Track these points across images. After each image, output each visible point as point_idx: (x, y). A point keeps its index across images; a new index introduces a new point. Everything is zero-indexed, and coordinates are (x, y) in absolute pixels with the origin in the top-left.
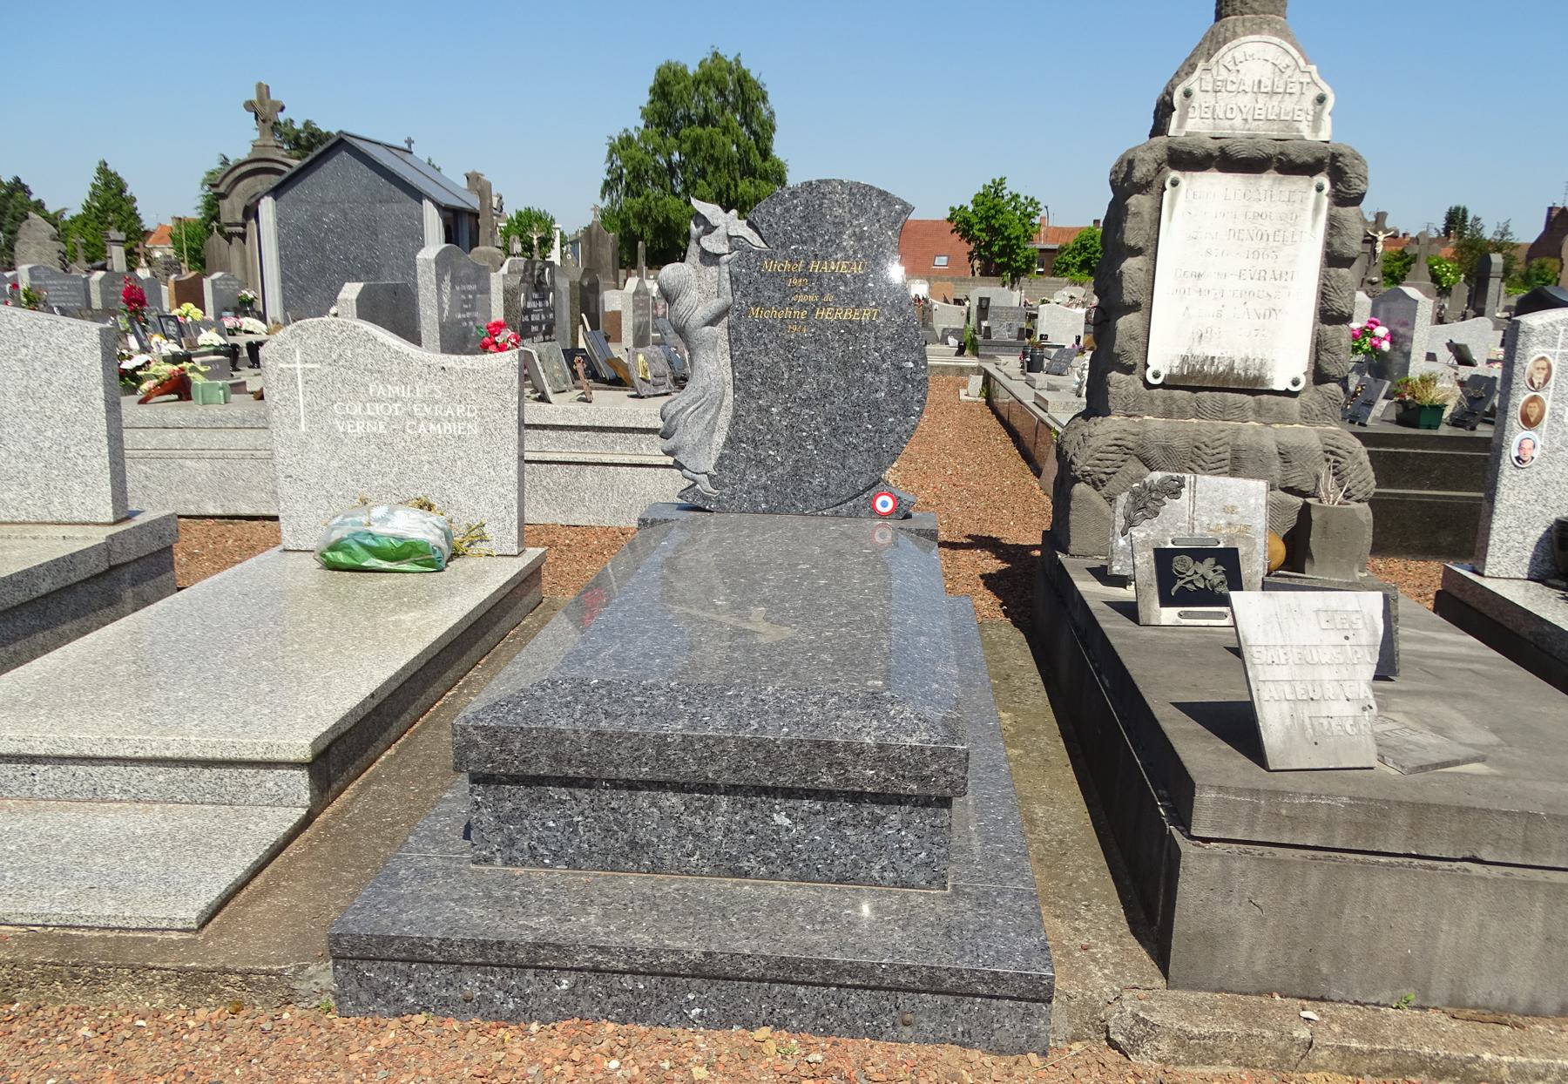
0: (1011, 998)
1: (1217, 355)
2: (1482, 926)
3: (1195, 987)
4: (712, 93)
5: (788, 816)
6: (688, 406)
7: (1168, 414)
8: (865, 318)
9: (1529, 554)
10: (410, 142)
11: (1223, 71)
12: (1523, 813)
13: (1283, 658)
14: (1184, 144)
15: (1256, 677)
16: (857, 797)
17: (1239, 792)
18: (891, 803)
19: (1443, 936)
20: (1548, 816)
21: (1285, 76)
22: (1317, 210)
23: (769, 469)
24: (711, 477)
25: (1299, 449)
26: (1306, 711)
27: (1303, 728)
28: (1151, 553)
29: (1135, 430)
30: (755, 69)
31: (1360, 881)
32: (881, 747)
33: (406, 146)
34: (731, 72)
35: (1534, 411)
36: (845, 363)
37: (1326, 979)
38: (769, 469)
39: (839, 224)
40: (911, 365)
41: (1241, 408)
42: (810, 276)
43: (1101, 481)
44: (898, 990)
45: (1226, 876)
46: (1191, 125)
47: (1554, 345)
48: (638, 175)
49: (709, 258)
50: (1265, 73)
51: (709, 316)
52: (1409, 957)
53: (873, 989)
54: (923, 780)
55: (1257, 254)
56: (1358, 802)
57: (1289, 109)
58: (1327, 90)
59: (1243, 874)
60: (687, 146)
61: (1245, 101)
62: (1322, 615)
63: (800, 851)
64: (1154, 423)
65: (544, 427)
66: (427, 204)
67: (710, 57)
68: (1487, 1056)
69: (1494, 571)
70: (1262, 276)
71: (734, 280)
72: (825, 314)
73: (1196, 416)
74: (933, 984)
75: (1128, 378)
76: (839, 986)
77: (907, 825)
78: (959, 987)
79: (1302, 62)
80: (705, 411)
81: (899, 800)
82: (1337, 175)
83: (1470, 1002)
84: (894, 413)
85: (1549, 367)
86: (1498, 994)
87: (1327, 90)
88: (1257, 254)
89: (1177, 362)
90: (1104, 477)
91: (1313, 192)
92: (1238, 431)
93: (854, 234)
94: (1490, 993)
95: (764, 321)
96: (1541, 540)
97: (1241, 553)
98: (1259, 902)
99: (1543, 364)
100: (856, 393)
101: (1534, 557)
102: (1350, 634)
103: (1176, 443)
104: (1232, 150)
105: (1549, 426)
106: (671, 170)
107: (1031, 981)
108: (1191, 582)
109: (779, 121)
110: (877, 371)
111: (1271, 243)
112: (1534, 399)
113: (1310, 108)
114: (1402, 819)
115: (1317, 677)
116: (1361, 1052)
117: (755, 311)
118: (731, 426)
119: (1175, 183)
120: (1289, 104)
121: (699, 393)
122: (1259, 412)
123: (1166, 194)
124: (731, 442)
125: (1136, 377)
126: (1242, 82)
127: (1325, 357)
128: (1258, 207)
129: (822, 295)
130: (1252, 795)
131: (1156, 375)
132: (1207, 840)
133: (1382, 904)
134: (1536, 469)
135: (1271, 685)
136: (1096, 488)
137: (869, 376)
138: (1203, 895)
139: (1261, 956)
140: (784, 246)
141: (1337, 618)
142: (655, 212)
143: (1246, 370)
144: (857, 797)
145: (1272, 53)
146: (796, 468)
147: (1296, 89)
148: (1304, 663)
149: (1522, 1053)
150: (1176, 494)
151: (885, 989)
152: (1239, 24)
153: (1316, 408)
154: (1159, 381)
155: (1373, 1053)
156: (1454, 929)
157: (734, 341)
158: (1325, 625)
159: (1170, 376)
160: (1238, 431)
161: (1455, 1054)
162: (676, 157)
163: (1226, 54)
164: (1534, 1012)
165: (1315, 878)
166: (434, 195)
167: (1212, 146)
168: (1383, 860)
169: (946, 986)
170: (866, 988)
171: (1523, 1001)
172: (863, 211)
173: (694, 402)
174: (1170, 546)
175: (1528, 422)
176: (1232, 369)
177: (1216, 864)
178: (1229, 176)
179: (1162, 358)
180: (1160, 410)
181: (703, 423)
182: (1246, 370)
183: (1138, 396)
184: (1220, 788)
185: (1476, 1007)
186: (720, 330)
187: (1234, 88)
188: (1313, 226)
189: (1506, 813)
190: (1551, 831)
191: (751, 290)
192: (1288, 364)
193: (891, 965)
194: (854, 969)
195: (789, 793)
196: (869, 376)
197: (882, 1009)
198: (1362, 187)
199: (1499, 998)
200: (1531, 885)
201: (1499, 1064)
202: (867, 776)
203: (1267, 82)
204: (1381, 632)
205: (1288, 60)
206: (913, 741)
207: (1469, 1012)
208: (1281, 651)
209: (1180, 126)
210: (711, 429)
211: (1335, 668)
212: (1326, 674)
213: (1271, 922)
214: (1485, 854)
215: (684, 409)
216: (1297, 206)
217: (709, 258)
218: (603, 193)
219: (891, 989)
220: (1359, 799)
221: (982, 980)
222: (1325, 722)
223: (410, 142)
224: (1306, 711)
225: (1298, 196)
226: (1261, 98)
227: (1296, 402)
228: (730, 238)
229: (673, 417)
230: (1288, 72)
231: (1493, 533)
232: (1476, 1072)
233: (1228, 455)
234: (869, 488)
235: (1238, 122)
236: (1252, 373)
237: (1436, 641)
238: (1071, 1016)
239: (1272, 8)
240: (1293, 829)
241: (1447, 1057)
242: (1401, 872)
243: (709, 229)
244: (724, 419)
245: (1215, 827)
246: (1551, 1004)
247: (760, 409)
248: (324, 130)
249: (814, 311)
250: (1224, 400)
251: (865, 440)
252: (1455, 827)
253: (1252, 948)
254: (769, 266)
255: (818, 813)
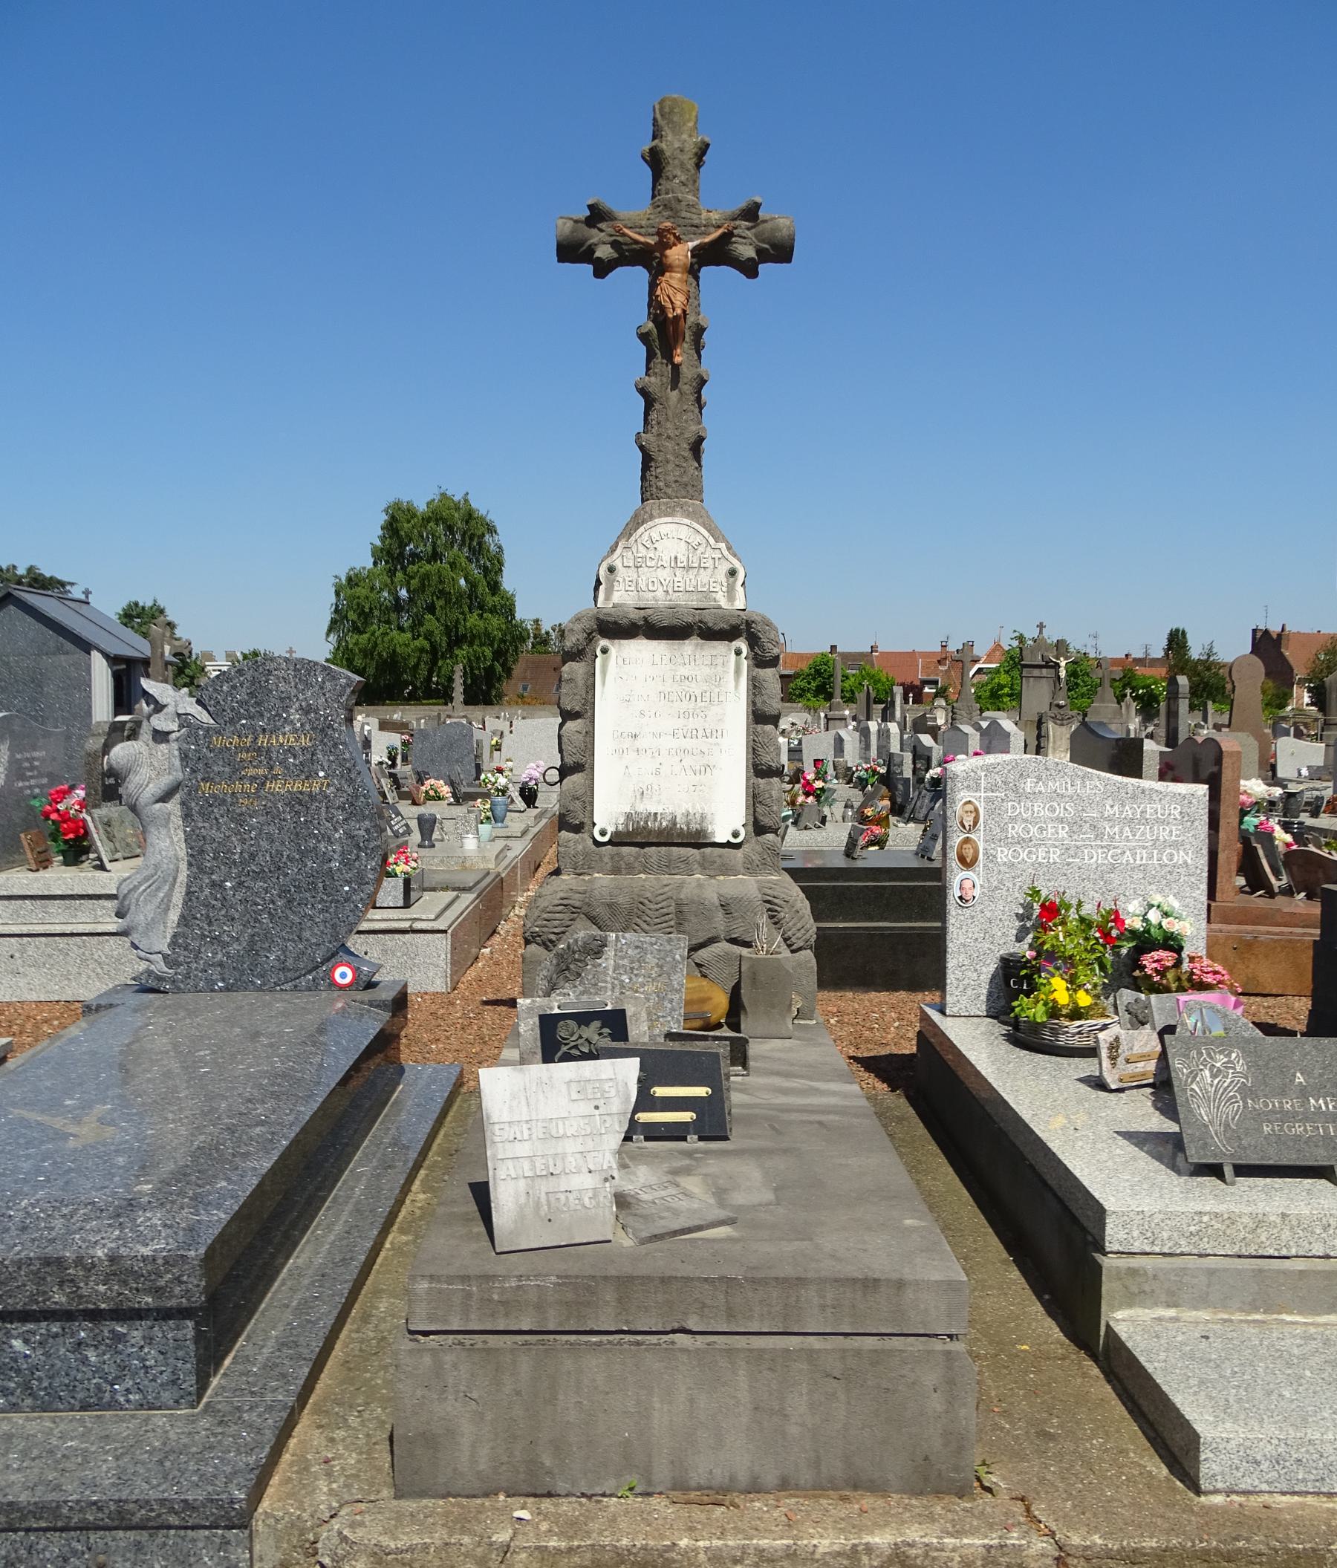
0: (205, 1528)
1: (660, 811)
2: (692, 1401)
3: (422, 1494)
4: (441, 529)
5: (26, 1341)
6: (140, 884)
7: (616, 871)
8: (316, 790)
9: (985, 991)
10: (87, 593)
11: (641, 548)
12: (721, 1278)
13: (526, 1134)
14: (609, 615)
15: (494, 1156)
16: (95, 1316)
17: (450, 1279)
18: (131, 1319)
19: (656, 1414)
20: (745, 1278)
21: (698, 552)
22: (738, 671)
23: (225, 945)
24: (165, 957)
25: (739, 900)
26: (543, 1187)
27: (538, 1205)
28: (537, 1020)
29: (581, 889)
30: (480, 505)
31: (568, 1364)
32: (113, 1259)
33: (83, 597)
34: (457, 508)
35: (969, 854)
36: (297, 834)
37: (549, 1473)
38: (225, 945)
39: (285, 700)
40: (362, 832)
41: (686, 861)
42: (259, 750)
43: (551, 941)
44: (88, 1529)
45: (438, 1371)
46: (622, 598)
47: (978, 790)
48: (365, 616)
49: (160, 736)
50: (681, 551)
51: (159, 793)
52: (628, 1440)
53: (62, 1530)
54: (158, 1292)
55: (687, 714)
56: (566, 1281)
57: (705, 581)
58: (737, 565)
59: (455, 1366)
60: (415, 583)
61: (664, 575)
62: (574, 1086)
63: (40, 1379)
64: (602, 880)
65: (99, 897)
66: (95, 654)
67: (437, 498)
68: (683, 1543)
69: (955, 1010)
70: (694, 734)
71: (184, 757)
72: (276, 787)
73: (644, 872)
74: (121, 1520)
75: (577, 836)
76: (28, 1530)
77: (149, 1340)
78: (149, 1519)
79: (711, 540)
80: (158, 889)
81: (137, 1315)
82: (753, 641)
83: (693, 1484)
84: (348, 883)
85: (976, 810)
86: (718, 1471)
87: (737, 565)
88: (687, 714)
89: (622, 820)
90: (553, 937)
91: (733, 656)
92: (681, 886)
93: (301, 708)
94: (711, 1472)
95: (214, 796)
96: (994, 977)
97: (629, 1014)
98: (475, 1395)
99: (970, 807)
100: (310, 864)
101: (990, 994)
102: (600, 1103)
103: (620, 900)
104: (653, 619)
105: (985, 866)
106: (398, 606)
107: (222, 1507)
108: (576, 1047)
109: (507, 558)
110: (330, 842)
111: (699, 704)
112: (967, 840)
113: (724, 580)
114: (609, 1295)
115: (560, 1151)
116: (558, 1551)
117: (205, 787)
118: (185, 903)
119: (605, 651)
120: (704, 577)
121: (151, 871)
122: (705, 865)
123: (598, 661)
124: (184, 920)
125: (586, 836)
126: (660, 558)
127: (760, 809)
128: (684, 671)
129: (271, 768)
130: (463, 1283)
131: (603, 833)
132: (426, 1334)
133: (598, 1390)
134: (979, 908)
135: (510, 1163)
136: (547, 948)
137: (322, 846)
138: (419, 1393)
139: (484, 1452)
140: (232, 721)
141: (589, 1087)
142: (380, 648)
143: (688, 824)
144: (95, 1316)
145: (684, 532)
146: (252, 943)
147: (710, 564)
148: (549, 1137)
149: (722, 1536)
150: (598, 953)
151: (75, 1529)
152: (655, 507)
153: (756, 858)
154: (606, 839)
155: (570, 1550)
156: (666, 1407)
157: (187, 816)
158: (575, 1096)
159: (616, 834)
160: (681, 886)
161: (651, 1543)
162: (403, 593)
163: (643, 533)
164: (755, 1488)
165: (525, 1365)
166: (102, 646)
167: (636, 616)
168: (594, 1339)
169: (136, 1519)
170: (55, 1529)
171: (743, 1478)
172: (308, 685)
173: (146, 879)
174: (556, 1011)
175: (967, 863)
176: (675, 824)
177: (427, 1360)
178: (655, 643)
179: (608, 813)
180: (609, 866)
181: (157, 901)
182: (688, 824)
183: (586, 854)
184: (432, 1278)
185: (699, 1488)
186: (173, 806)
187: (653, 563)
188: (736, 687)
189: (706, 1280)
190: (750, 1294)
191: (201, 765)
192: (727, 817)
193: (78, 1502)
194: (40, 1510)
195: (25, 1316)
196: (322, 846)
197: (75, 1553)
198: (776, 651)
199: (720, 1476)
200: (730, 1352)
201: (696, 1550)
202: (99, 1292)
203: (682, 558)
204: (633, 1099)
205: (699, 539)
206: (146, 1251)
207: (693, 1495)
208: (525, 1126)
209: (607, 598)
210: (165, 907)
211: (580, 1140)
212: (570, 1147)
213: (489, 1416)
214: (692, 1324)
215: (136, 888)
216: (719, 668)
217: (160, 736)
218: (330, 630)
219: (81, 1529)
220: (567, 1277)
221: (172, 1511)
222: (562, 1197)
223: (87, 593)
224: (543, 1187)
225: (720, 660)
226: (679, 572)
227: (739, 854)
228: (179, 715)
229: (125, 897)
230: (701, 549)
231: (949, 972)
232: (675, 1561)
233: (672, 909)
234: (328, 960)
235: (660, 594)
236: (694, 827)
237: (817, 1091)
238: (279, 1540)
239: (683, 493)
240: (506, 1315)
241: (644, 1548)
242: (607, 1351)
243: (159, 708)
244: (178, 897)
245: (431, 1319)
246: (771, 1478)
247: (213, 884)
248: (48, 575)
249: (263, 784)
250: (669, 855)
251: (321, 911)
252: (660, 1297)
253: (473, 1446)
254: (217, 741)
255: (56, 1336)
